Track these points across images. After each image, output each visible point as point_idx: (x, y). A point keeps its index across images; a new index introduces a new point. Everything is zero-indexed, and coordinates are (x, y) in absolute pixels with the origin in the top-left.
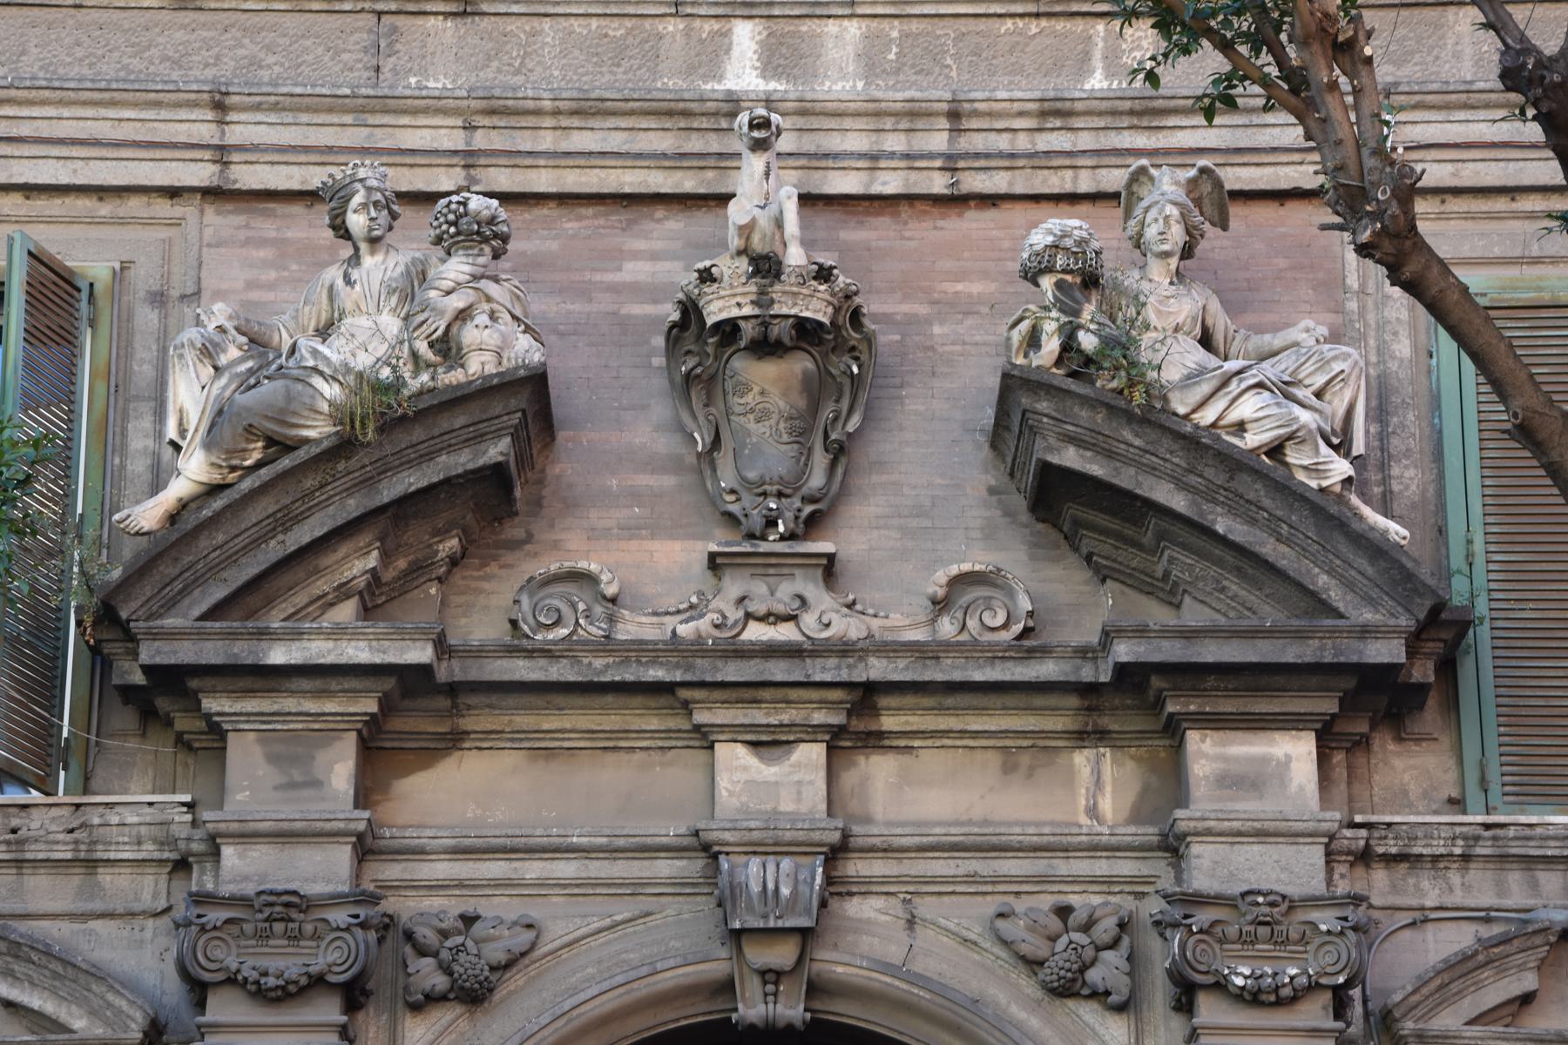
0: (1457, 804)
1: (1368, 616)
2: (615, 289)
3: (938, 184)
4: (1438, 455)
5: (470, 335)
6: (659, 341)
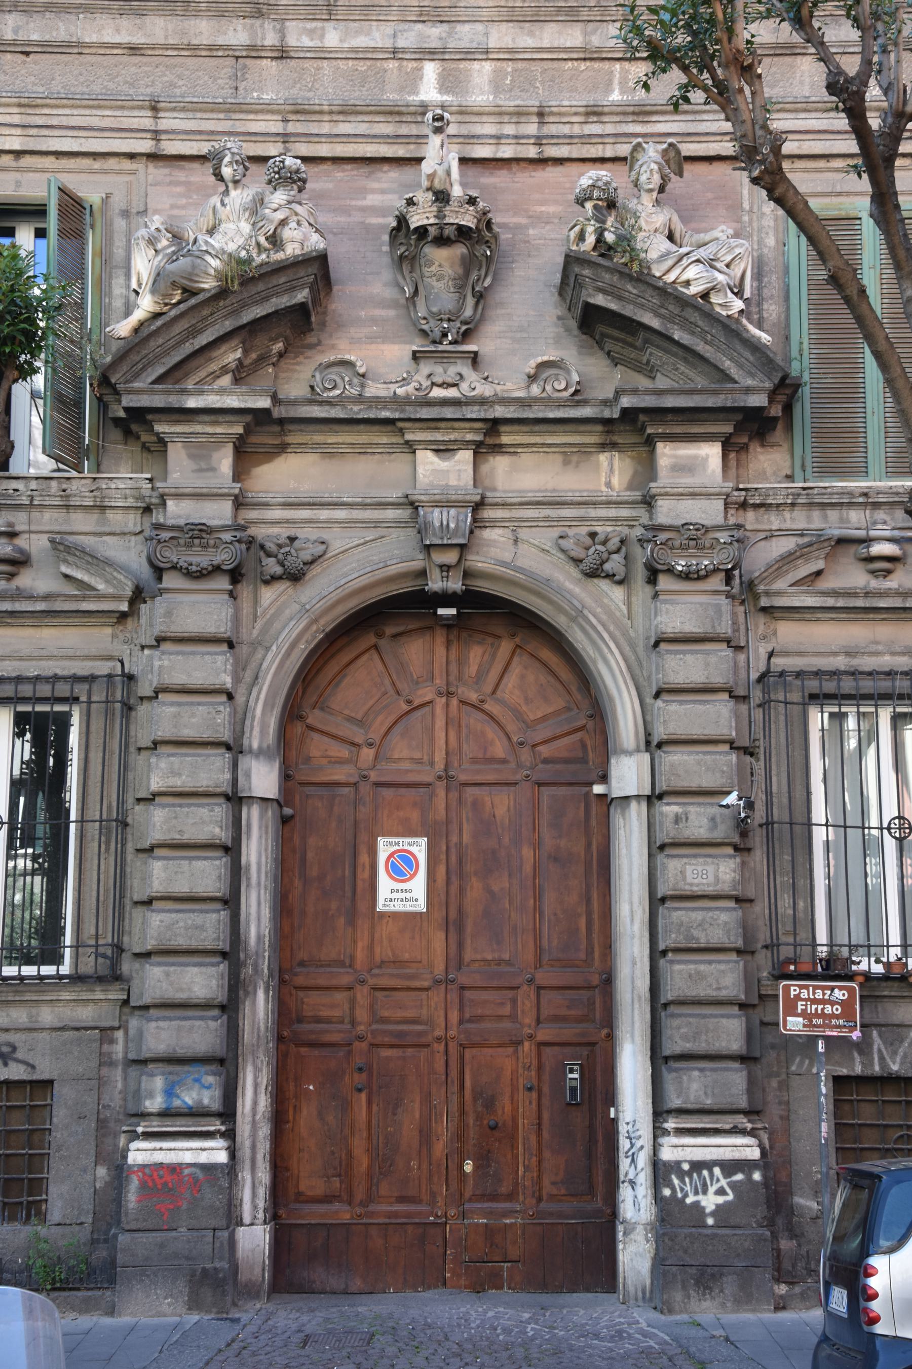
0: (790, 478)
1: (750, 382)
2: (363, 209)
3: (532, 152)
6: (386, 238)
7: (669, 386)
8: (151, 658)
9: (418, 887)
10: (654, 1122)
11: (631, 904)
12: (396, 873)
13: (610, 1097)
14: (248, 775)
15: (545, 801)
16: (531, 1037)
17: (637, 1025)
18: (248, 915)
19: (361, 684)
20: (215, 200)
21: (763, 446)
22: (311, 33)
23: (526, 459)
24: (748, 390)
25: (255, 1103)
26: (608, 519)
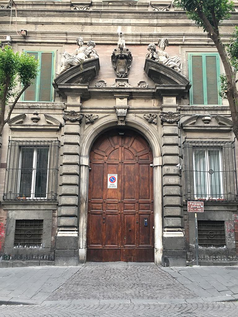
0: (189, 105)
1: (182, 84)
2: (106, 53)
3: (139, 43)
4: (188, 71)
5: (91, 55)
6: (111, 58)
7: (165, 86)
8: (63, 138)
9: (116, 183)
10: (162, 229)
11: (158, 186)
12: (111, 181)
13: (153, 224)
14: (82, 161)
15: (141, 167)
16: (137, 213)
17: (159, 210)
18: (82, 188)
19: (105, 146)
20: (77, 49)
21: (183, 99)
22: (97, 20)
23: (138, 100)
24: (181, 86)
25: (83, 225)
26: (154, 112)
